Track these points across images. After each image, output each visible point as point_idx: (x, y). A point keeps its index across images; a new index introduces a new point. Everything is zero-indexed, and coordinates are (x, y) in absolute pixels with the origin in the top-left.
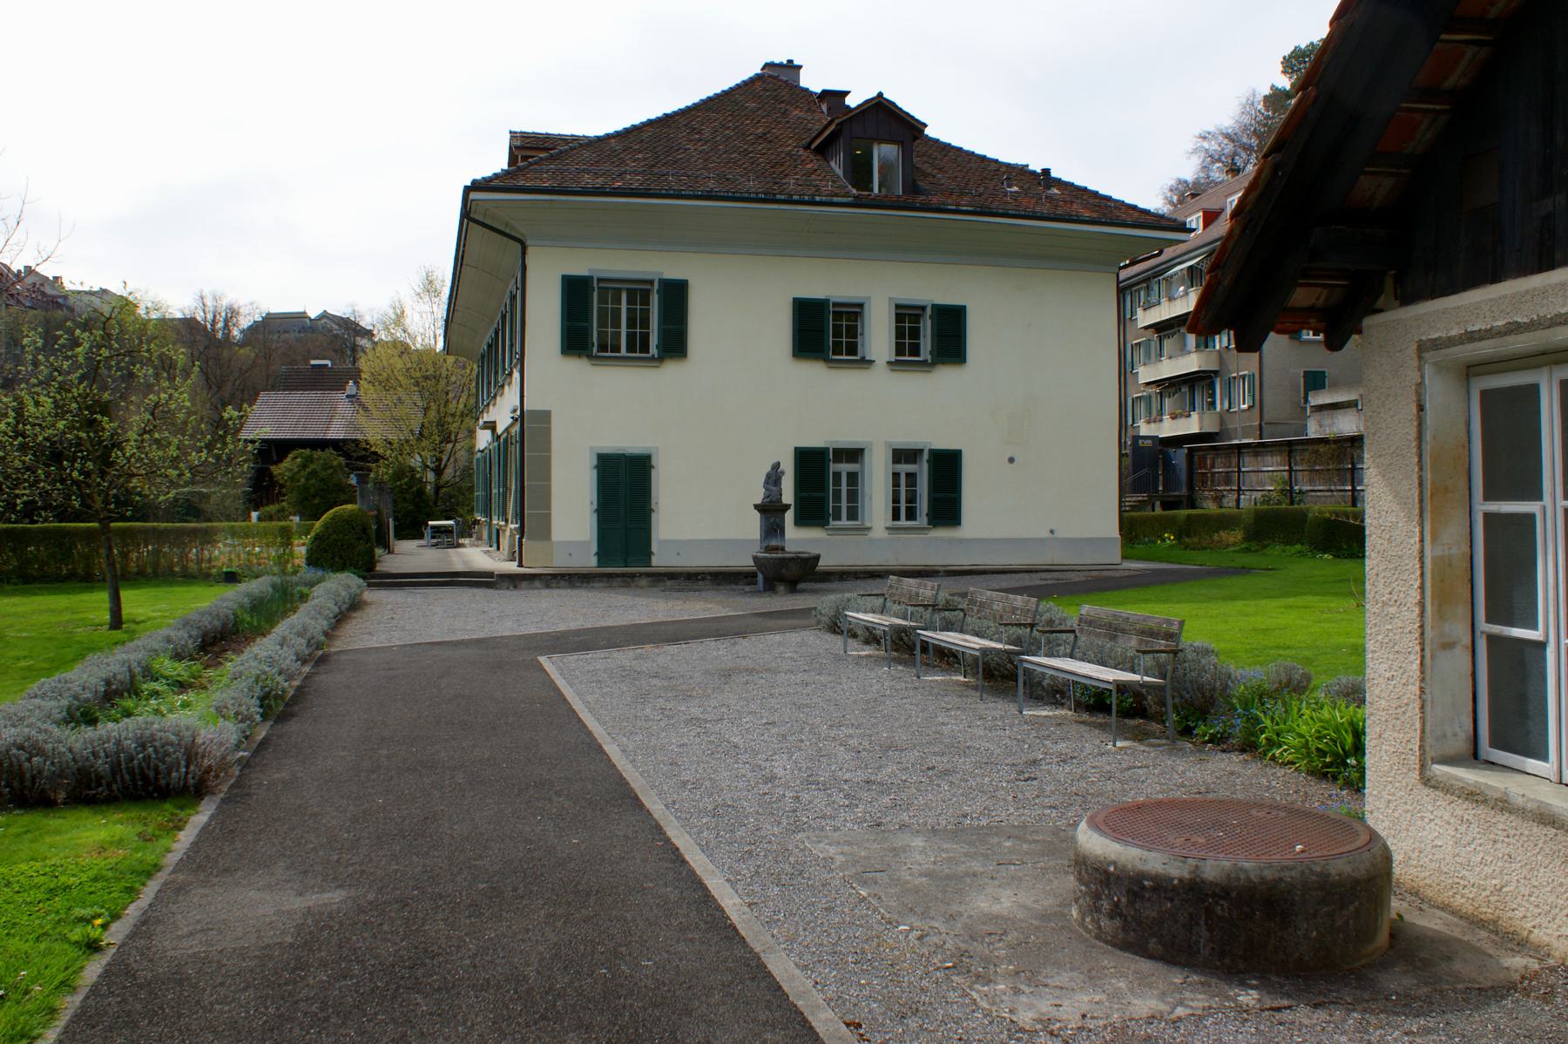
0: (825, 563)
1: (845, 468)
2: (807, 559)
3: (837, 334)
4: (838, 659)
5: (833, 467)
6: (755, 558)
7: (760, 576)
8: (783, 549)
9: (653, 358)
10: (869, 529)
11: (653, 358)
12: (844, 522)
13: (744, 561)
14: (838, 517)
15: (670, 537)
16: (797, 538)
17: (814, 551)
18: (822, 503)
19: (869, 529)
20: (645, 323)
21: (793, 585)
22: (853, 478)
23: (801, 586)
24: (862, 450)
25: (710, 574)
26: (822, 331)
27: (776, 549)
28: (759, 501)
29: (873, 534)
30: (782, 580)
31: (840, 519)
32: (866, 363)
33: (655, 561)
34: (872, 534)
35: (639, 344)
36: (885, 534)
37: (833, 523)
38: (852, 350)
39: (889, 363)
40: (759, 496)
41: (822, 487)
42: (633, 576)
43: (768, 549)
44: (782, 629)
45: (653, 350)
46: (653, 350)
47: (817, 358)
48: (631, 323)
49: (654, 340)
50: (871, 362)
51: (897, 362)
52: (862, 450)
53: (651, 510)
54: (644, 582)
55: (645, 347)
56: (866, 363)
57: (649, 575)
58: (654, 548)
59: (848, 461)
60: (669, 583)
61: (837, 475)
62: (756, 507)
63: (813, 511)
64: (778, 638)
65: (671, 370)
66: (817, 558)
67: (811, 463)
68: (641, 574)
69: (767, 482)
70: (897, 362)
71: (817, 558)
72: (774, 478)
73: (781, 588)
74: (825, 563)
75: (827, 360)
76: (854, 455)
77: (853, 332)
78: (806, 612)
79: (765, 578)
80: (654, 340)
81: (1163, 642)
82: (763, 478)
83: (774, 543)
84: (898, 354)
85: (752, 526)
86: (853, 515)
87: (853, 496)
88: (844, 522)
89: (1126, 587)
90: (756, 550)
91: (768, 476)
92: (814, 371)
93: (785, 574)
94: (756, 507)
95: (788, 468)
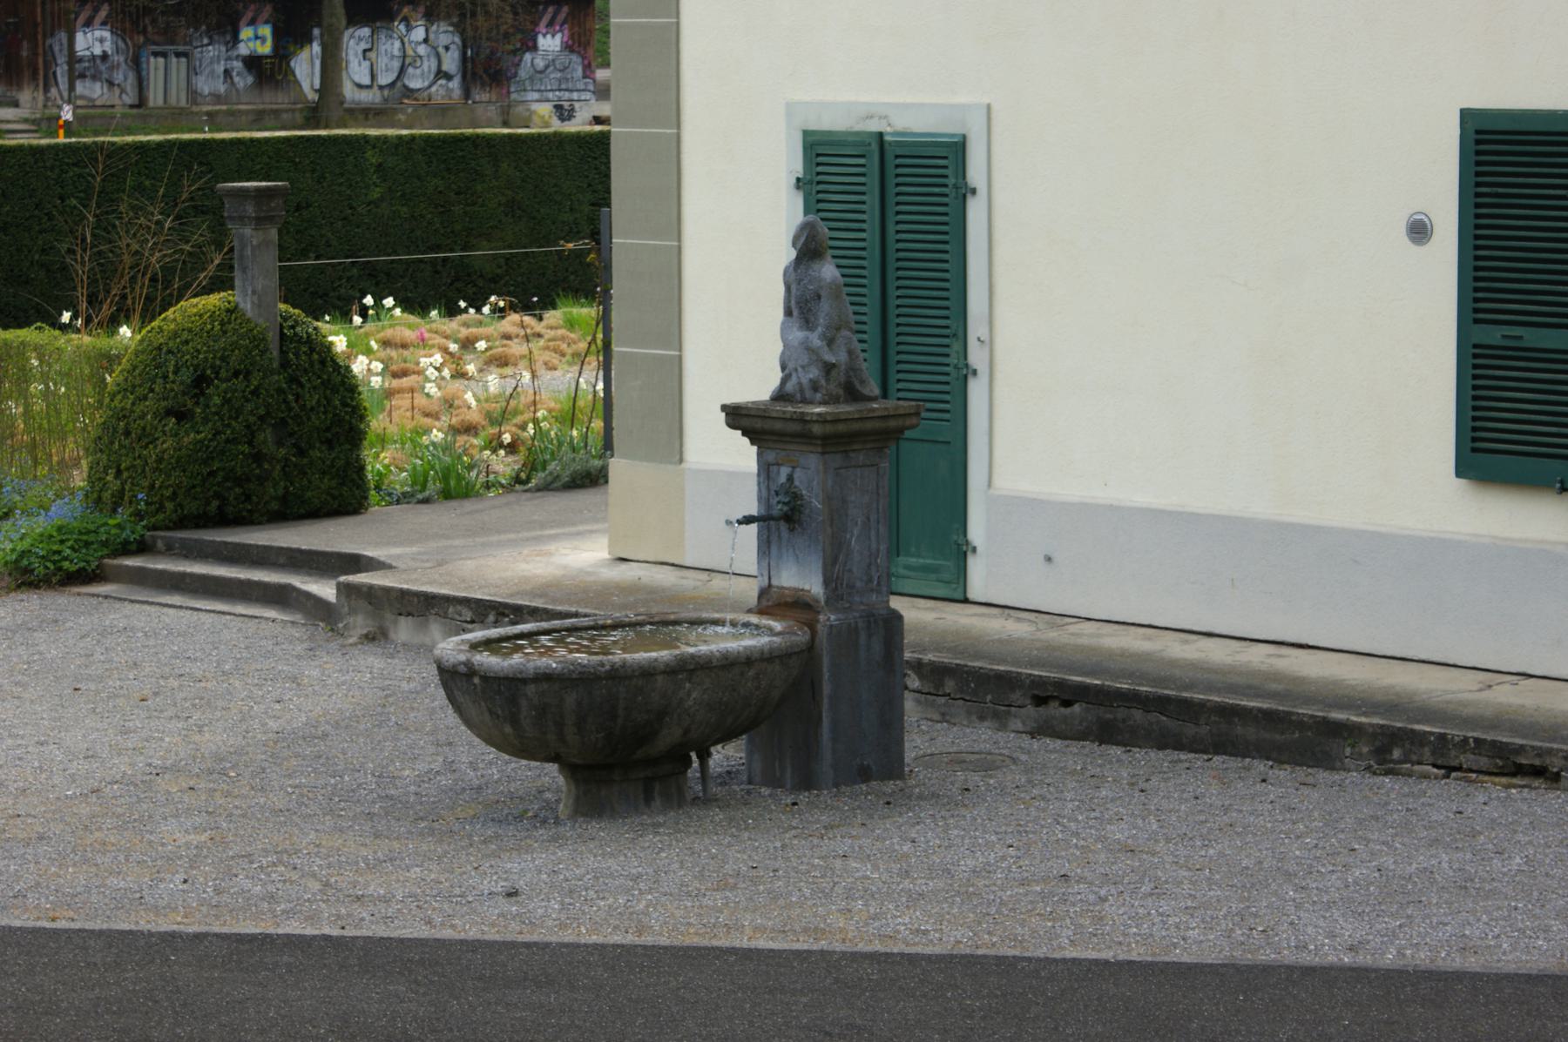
33: (980, 580)
53: (965, 373)
58: (977, 530)
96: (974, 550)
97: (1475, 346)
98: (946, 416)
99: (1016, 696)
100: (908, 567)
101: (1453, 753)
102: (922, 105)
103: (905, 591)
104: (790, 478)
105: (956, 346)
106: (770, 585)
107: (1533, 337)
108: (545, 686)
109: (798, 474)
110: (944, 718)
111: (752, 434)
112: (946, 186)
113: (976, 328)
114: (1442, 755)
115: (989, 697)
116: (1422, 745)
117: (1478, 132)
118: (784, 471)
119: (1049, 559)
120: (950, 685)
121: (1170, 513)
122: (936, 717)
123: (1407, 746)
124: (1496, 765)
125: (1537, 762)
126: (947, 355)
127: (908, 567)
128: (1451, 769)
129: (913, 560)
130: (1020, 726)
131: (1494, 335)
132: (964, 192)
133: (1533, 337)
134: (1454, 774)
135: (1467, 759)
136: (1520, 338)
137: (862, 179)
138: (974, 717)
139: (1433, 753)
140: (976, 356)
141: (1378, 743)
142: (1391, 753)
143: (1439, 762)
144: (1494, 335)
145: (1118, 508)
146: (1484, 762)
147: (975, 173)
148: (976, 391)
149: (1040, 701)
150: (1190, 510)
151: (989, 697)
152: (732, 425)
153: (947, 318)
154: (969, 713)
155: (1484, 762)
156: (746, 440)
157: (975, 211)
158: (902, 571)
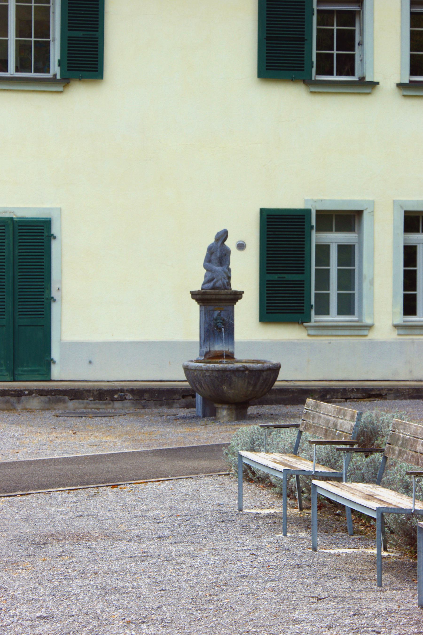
0: (287, 376)
1: (335, 238)
2: (260, 371)
3: (324, 41)
4: (223, 518)
5: (317, 238)
6: (187, 369)
7: (199, 398)
8: (230, 356)
9: (53, 81)
10: (369, 327)
11: (53, 81)
12: (333, 317)
13: (173, 374)
14: (323, 309)
15: (76, 338)
16: (252, 336)
17: (272, 359)
18: (302, 287)
19: (369, 327)
20: (44, 29)
21: (240, 409)
22: (347, 253)
23: (252, 410)
24: (359, 213)
25: (132, 391)
26: (302, 39)
27: (219, 356)
28: (198, 287)
29: (374, 335)
30: (224, 401)
31: (327, 313)
32: (367, 86)
33: (56, 372)
34: (373, 335)
35: (33, 59)
36: (393, 335)
37: (314, 318)
38: (347, 65)
39: (400, 86)
40: (197, 280)
41: (302, 267)
42: (19, 394)
43: (211, 356)
44: (194, 473)
45: (55, 69)
46: (55, 69)
47: (293, 80)
48: (22, 30)
49: (55, 53)
50: (374, 84)
51: (412, 85)
52: (359, 213)
53: (51, 299)
54: (35, 402)
55: (43, 65)
56: (367, 86)
57: (41, 393)
58: (55, 354)
59: (339, 229)
60: (72, 404)
61: (323, 250)
62: (194, 295)
63: (284, 300)
64: (163, 487)
65: (81, 96)
66: (275, 370)
67: (285, 235)
68: (31, 392)
69: (208, 260)
70: (412, 85)
71: (275, 370)
72: (218, 255)
73: (224, 412)
74: (287, 376)
75: (308, 82)
76: (348, 219)
77: (348, 41)
78: (212, 451)
79: (204, 399)
80: (55, 53)
81: (295, 491)
82: (204, 252)
83: (218, 347)
84: (413, 72)
85: (187, 324)
86: (347, 306)
87: (347, 280)
88: (333, 317)
89: (390, 390)
90: (193, 355)
91: (211, 250)
92: (289, 98)
93: (233, 391)
94: (194, 295)
95: (246, 233)
96: (54, 363)
97: (267, 281)
98: (43, 316)
99: (176, 396)
100: (22, 371)
101: (349, 394)
102: (29, 208)
103: (22, 379)
104: (219, 315)
105: (47, 292)
106: (210, 351)
107: (288, 277)
108: (268, 372)
109: (223, 313)
110: (144, 407)
111: (198, 301)
112: (43, 236)
113: (54, 286)
114: (345, 395)
115: (164, 398)
116: (338, 393)
117: (268, 215)
118: (216, 313)
119: (90, 362)
120: (146, 396)
121: (143, 342)
122: (141, 407)
123: (332, 393)
124: (363, 396)
125: (378, 393)
126: (43, 295)
127: (22, 371)
128: (346, 399)
129: (26, 368)
130: (178, 406)
131: (275, 277)
132: (51, 237)
133: (288, 277)
134: (348, 400)
135: (352, 395)
136: (284, 277)
137: (3, 234)
138: (158, 406)
139: (342, 395)
140: (54, 293)
141: (321, 394)
142: (326, 397)
143: (344, 397)
144: (275, 277)
145: (120, 342)
146: (359, 395)
147: (54, 231)
148: (55, 307)
149: (184, 397)
150: (151, 341)
151: (164, 398)
152: (193, 298)
153: (43, 282)
154: (155, 405)
155: (359, 395)
156: (196, 303)
157: (54, 245)
158: (20, 373)
